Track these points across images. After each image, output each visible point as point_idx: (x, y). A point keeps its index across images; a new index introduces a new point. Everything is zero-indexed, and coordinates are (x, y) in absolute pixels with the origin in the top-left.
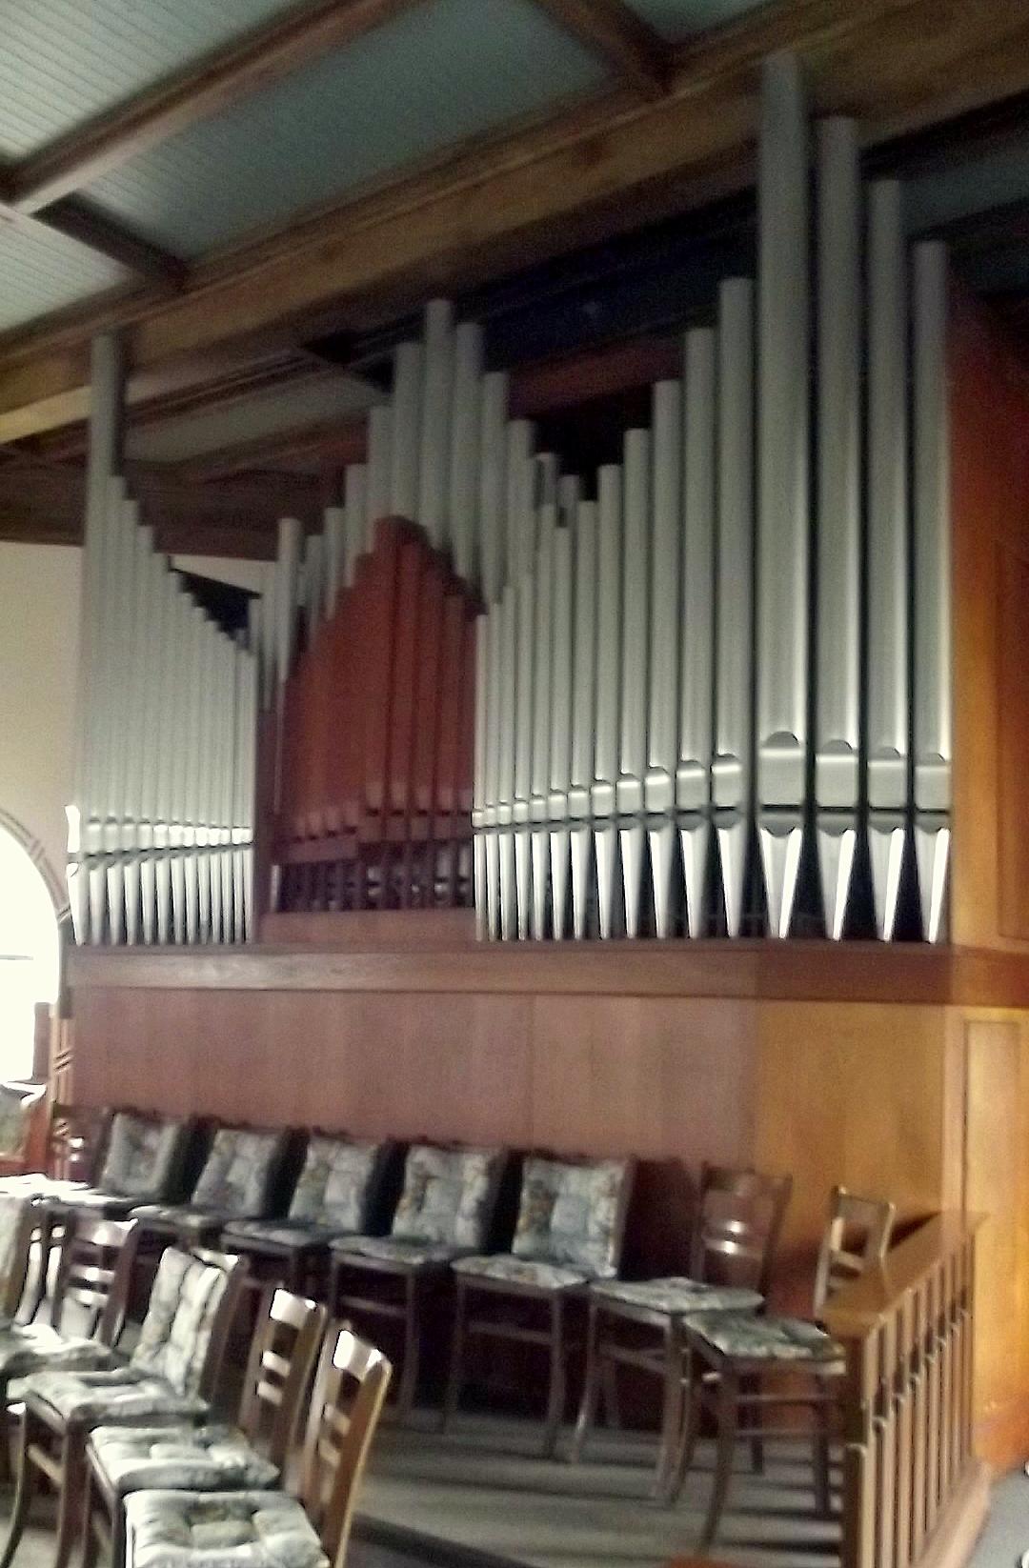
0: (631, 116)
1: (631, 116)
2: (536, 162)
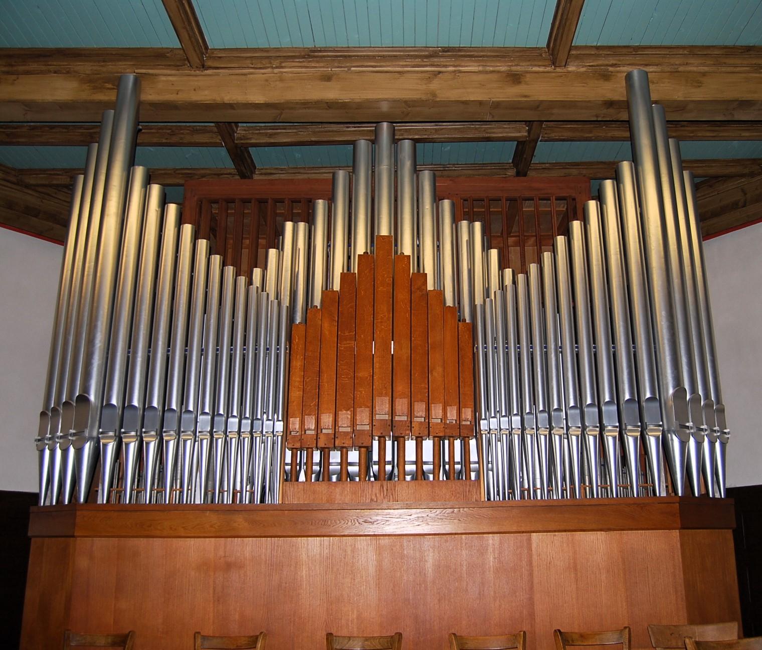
0: (541, 69)
1: (541, 69)
2: (480, 72)
